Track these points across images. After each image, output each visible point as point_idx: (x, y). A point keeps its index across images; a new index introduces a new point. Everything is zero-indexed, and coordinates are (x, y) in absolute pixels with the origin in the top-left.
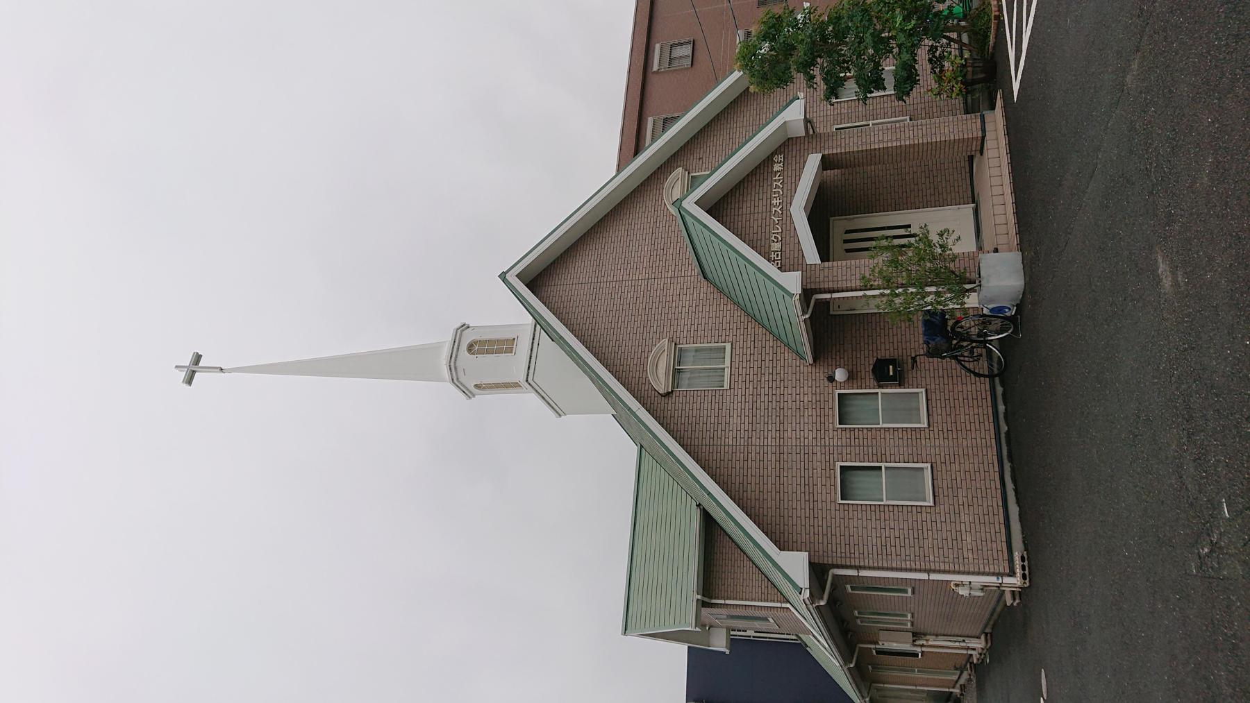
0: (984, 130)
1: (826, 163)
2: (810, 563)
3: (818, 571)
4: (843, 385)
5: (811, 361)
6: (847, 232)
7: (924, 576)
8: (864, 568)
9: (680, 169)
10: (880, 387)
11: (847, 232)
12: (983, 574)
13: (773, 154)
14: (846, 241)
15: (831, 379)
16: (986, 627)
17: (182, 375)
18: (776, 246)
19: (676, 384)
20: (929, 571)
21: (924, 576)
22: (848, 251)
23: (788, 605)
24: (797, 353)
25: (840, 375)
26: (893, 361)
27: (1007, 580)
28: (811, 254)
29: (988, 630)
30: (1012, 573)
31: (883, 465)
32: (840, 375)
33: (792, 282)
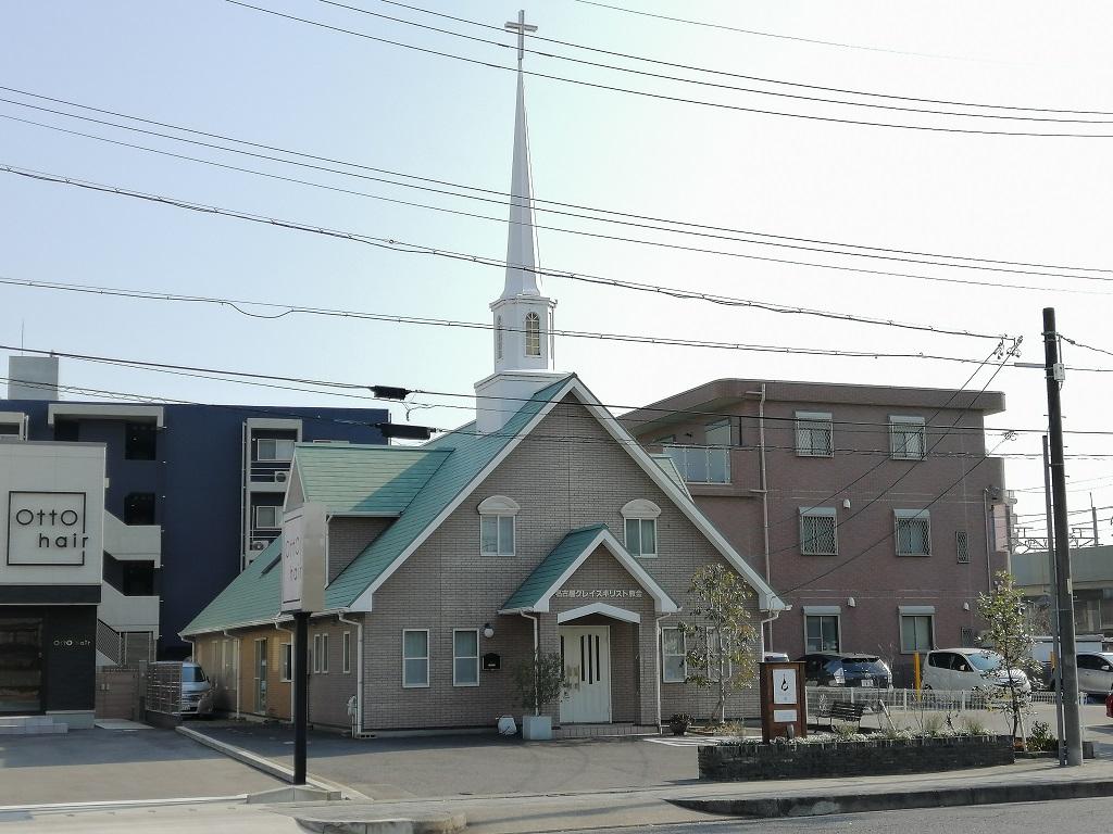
0: (644, 726)
1: (635, 625)
2: (232, 417)
3: (360, 616)
4: (482, 633)
5: (501, 612)
6: (597, 638)
7: (359, 680)
8: (363, 645)
9: (660, 511)
10: (481, 657)
11: (597, 638)
12: (363, 714)
13: (642, 589)
14: (590, 637)
15: (487, 626)
16: (318, 724)
17: (516, 20)
18: (572, 593)
19: (487, 518)
20: (363, 683)
21: (359, 680)
22: (582, 638)
23: (327, 584)
24: (506, 603)
25: (489, 632)
26: (498, 666)
27: (359, 728)
28: (564, 617)
29: (315, 726)
30: (363, 730)
31: (428, 658)
32: (489, 632)
33: (542, 605)
